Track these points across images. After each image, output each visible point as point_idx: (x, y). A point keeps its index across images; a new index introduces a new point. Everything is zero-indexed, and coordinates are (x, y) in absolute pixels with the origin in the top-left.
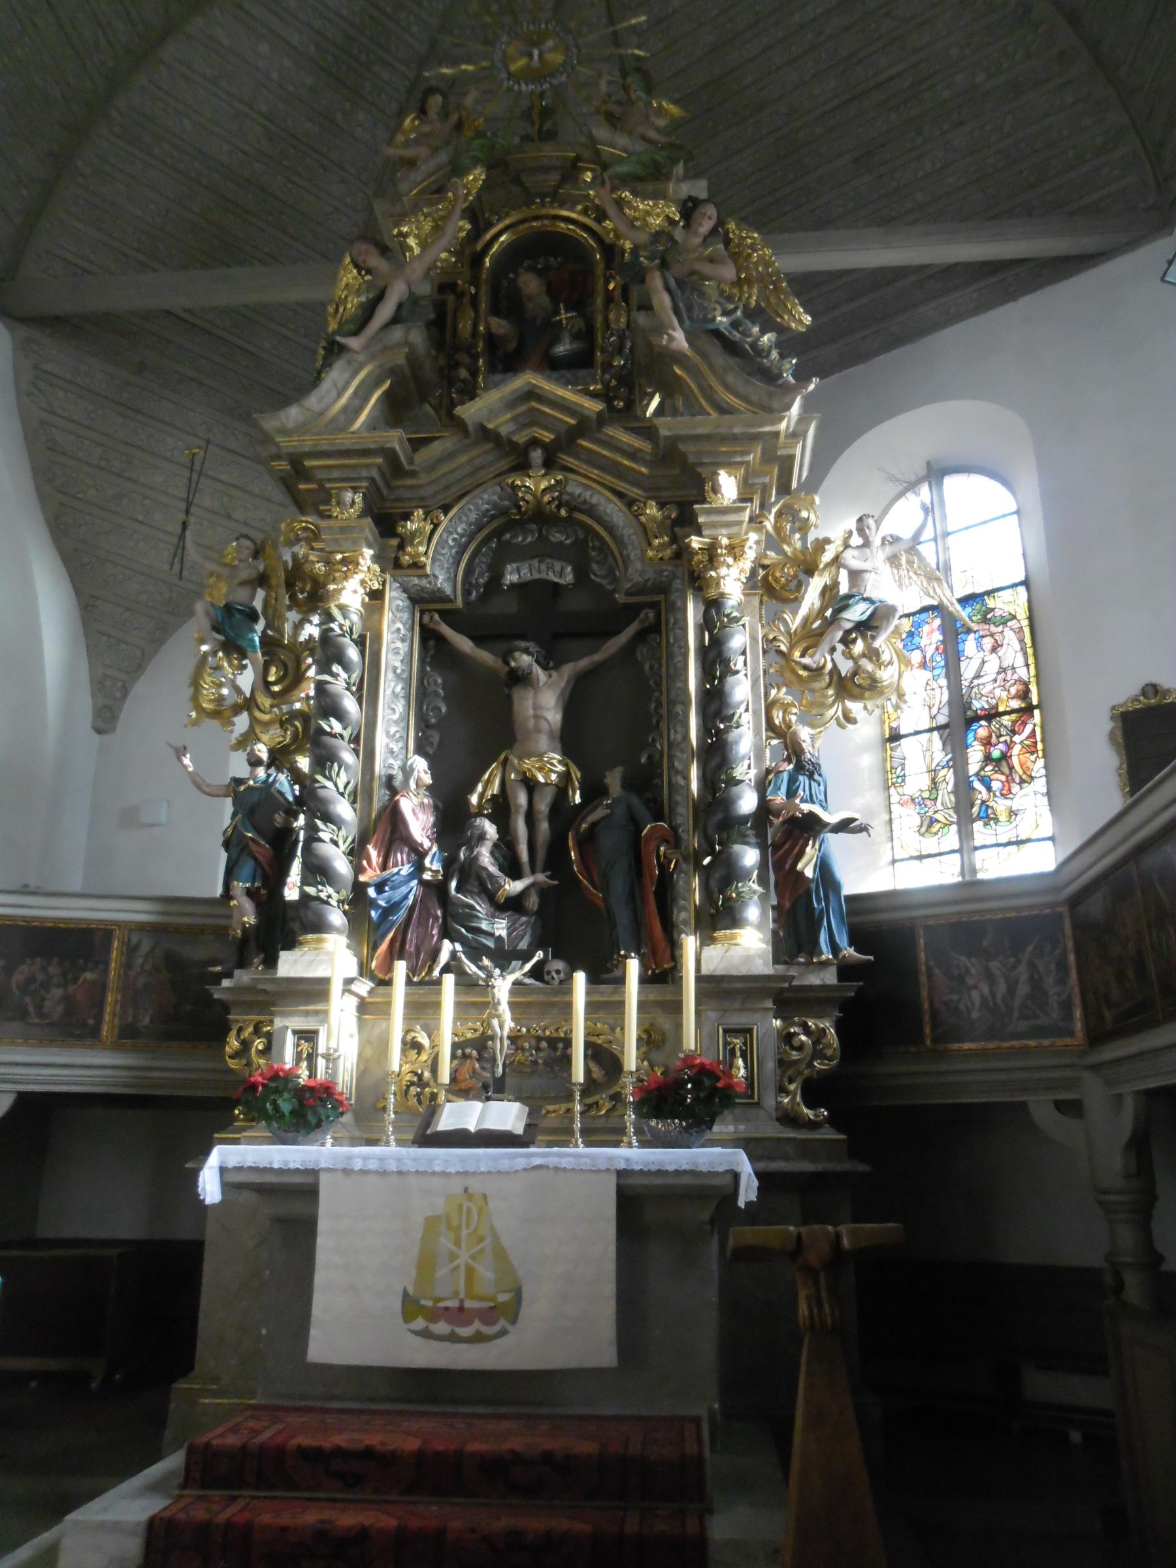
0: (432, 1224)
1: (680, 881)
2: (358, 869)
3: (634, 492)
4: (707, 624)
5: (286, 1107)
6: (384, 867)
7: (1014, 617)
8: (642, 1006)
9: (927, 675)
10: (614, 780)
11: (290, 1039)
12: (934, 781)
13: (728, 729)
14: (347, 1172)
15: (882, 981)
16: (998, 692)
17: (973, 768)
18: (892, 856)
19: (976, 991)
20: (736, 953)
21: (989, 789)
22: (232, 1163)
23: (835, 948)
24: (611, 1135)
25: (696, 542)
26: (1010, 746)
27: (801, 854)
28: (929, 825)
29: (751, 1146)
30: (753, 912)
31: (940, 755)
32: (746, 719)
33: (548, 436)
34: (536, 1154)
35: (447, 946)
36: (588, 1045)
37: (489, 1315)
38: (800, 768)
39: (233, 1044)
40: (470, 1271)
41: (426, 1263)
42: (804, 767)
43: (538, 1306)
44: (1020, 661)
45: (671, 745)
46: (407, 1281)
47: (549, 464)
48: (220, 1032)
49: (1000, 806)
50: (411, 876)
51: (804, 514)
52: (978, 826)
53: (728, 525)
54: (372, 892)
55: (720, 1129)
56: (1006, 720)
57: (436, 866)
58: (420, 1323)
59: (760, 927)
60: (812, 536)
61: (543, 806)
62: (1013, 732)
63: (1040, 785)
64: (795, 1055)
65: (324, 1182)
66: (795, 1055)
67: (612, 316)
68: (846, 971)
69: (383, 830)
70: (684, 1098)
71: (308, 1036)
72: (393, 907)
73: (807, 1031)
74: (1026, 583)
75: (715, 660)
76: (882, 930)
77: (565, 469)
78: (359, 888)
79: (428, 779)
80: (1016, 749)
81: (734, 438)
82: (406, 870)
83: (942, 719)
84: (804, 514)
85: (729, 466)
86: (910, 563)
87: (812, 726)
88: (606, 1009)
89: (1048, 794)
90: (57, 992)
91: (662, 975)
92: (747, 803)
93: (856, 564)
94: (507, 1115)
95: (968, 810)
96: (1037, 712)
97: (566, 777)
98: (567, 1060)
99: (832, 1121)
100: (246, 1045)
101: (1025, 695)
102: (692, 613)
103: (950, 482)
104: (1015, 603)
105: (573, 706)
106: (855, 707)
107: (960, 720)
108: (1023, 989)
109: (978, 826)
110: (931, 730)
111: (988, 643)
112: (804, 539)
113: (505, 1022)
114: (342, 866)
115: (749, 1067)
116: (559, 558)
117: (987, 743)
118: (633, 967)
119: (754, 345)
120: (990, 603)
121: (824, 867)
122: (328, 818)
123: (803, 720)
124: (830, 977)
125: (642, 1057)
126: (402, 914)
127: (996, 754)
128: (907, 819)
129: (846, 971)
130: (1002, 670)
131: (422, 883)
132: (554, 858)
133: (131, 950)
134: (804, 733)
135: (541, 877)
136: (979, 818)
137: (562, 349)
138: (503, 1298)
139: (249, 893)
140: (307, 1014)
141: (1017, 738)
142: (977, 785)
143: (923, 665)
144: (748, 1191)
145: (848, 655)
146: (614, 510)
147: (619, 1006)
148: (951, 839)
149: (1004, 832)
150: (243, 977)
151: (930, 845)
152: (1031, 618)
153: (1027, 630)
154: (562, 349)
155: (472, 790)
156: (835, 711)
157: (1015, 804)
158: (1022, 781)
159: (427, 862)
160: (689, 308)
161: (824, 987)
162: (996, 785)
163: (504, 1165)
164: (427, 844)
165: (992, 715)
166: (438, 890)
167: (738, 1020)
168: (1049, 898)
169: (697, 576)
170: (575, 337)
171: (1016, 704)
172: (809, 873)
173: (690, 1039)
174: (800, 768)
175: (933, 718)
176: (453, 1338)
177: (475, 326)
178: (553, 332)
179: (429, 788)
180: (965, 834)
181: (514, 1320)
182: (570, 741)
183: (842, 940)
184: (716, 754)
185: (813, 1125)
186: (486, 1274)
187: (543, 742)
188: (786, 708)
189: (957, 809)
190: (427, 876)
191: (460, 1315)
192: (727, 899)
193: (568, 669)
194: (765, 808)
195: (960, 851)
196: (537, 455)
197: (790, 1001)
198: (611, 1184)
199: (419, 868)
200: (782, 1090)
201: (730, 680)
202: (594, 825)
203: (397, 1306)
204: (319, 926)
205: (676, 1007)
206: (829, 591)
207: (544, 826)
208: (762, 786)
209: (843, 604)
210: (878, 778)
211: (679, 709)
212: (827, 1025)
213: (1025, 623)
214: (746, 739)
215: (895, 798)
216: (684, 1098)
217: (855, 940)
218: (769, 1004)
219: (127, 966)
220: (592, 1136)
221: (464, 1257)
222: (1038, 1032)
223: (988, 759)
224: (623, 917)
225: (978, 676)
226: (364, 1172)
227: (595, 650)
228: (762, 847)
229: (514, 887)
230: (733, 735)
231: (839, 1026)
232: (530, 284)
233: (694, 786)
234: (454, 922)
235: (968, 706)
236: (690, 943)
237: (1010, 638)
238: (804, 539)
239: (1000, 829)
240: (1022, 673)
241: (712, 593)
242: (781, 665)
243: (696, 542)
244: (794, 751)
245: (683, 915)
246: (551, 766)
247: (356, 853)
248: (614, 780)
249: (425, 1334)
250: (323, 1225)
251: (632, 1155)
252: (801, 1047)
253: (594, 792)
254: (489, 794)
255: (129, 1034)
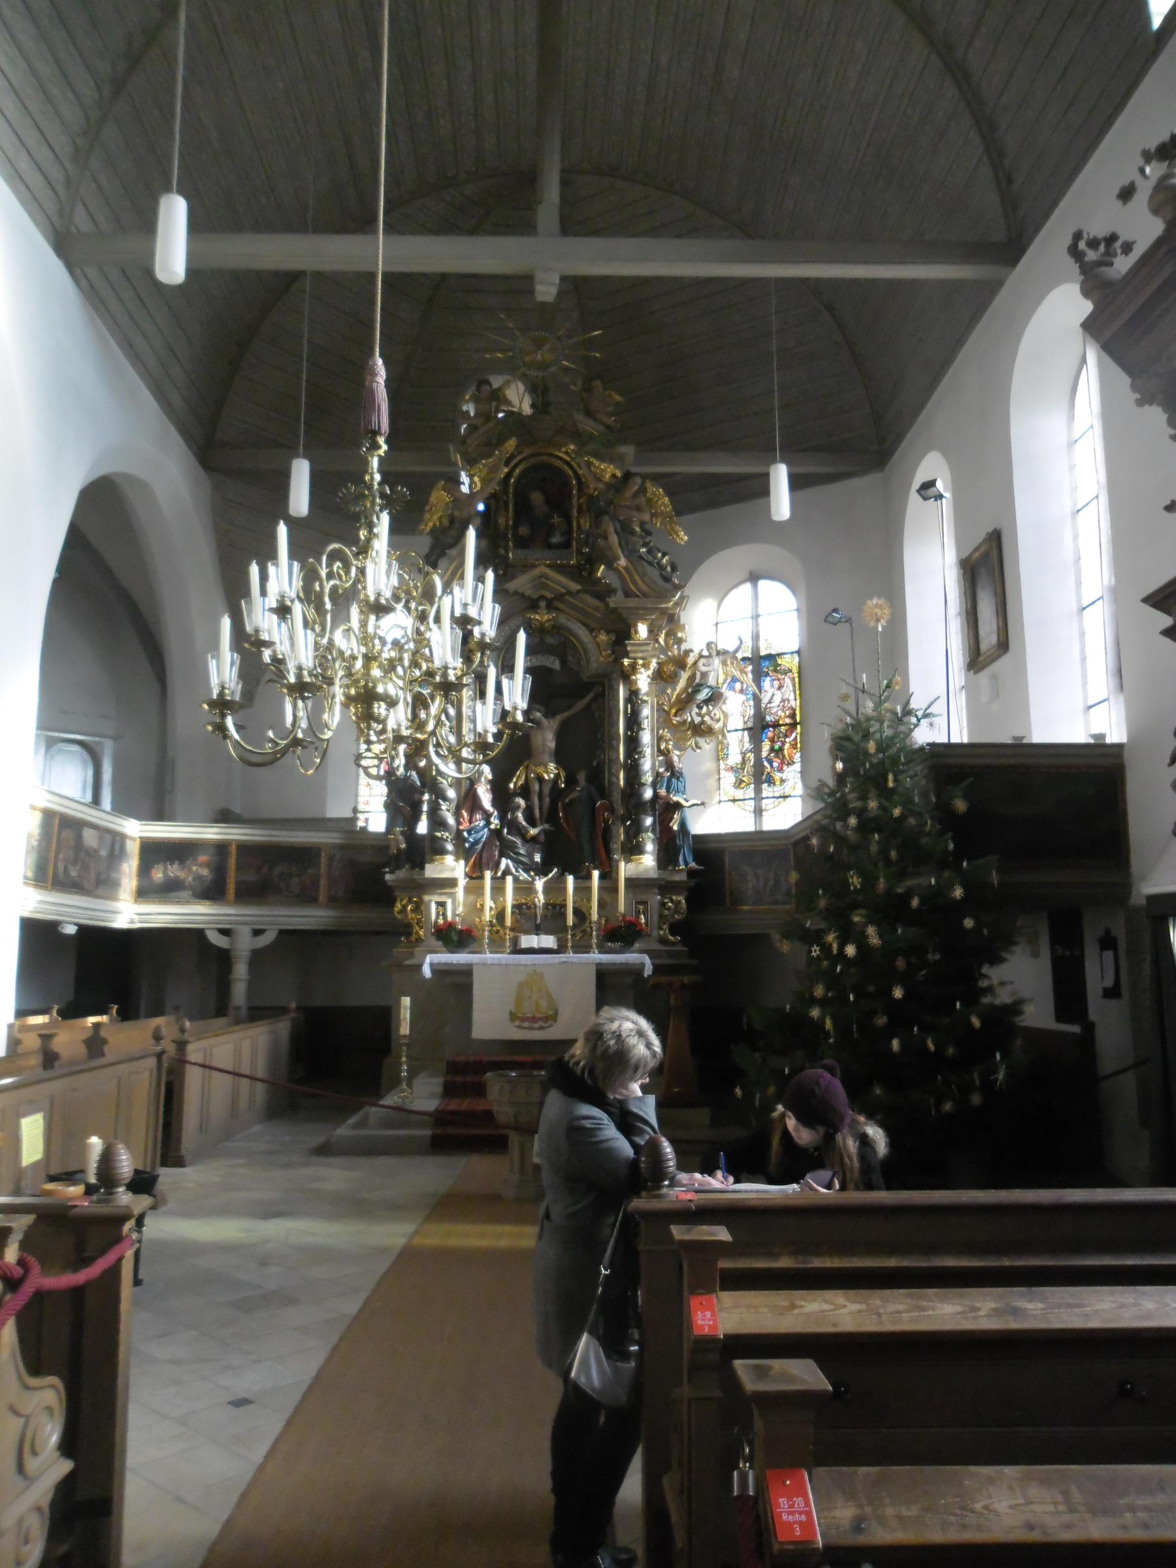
0: (521, 985)
1: (614, 829)
2: (458, 823)
3: (593, 625)
4: (628, 700)
5: (455, 938)
6: (470, 822)
7: (790, 671)
8: (600, 888)
9: (742, 697)
10: (582, 777)
11: (433, 906)
12: (743, 759)
13: (640, 758)
14: (485, 965)
15: (710, 870)
16: (780, 713)
17: (764, 754)
18: (719, 812)
19: (751, 881)
20: (641, 868)
21: (772, 766)
22: (436, 961)
23: (686, 863)
24: (586, 949)
25: (626, 662)
26: (784, 743)
27: (672, 818)
28: (739, 784)
29: (652, 954)
30: (650, 847)
31: (747, 745)
32: (648, 751)
33: (549, 595)
34: (562, 957)
35: (504, 861)
36: (574, 908)
37: (546, 1019)
38: (673, 775)
39: (398, 906)
40: (537, 1003)
41: (520, 999)
42: (675, 774)
43: (564, 1016)
44: (792, 697)
45: (610, 760)
46: (510, 1006)
47: (550, 607)
48: (392, 902)
49: (777, 776)
50: (485, 826)
51: (680, 635)
52: (765, 786)
53: (642, 651)
54: (465, 834)
55: (637, 945)
56: (783, 729)
57: (497, 821)
58: (517, 1023)
59: (652, 854)
60: (684, 647)
61: (546, 790)
62: (786, 736)
63: (797, 767)
64: (666, 912)
65: (475, 968)
66: (666, 912)
67: (582, 521)
68: (691, 873)
69: (468, 803)
70: (621, 934)
71: (441, 905)
72: (476, 842)
73: (672, 901)
74: (798, 652)
75: (634, 722)
76: (712, 853)
77: (557, 609)
78: (459, 833)
79: (490, 777)
80: (787, 746)
81: (646, 609)
82: (482, 823)
83: (750, 725)
84: (680, 635)
85: (643, 619)
86: (732, 663)
87: (680, 750)
88: (583, 890)
89: (801, 772)
90: (296, 880)
91: (609, 876)
92: (648, 794)
93: (704, 669)
94: (549, 941)
95: (760, 777)
96: (799, 727)
97: (557, 776)
98: (563, 916)
99: (683, 942)
100: (405, 907)
101: (793, 716)
102: (622, 692)
103: (762, 583)
104: (790, 662)
105: (560, 736)
106: (701, 741)
107: (759, 726)
108: (771, 882)
109: (765, 786)
110: (743, 730)
111: (776, 683)
112: (679, 649)
113: (541, 898)
114: (451, 821)
115: (646, 919)
116: (552, 654)
117: (772, 741)
118: (596, 874)
119: (659, 563)
120: (779, 661)
121: (683, 824)
122: (445, 799)
123: (676, 747)
124: (683, 877)
125: (600, 916)
126: (479, 846)
127: (777, 747)
128: (728, 778)
129: (691, 873)
130: (783, 701)
131: (490, 830)
132: (551, 817)
133: (331, 858)
134: (675, 756)
135: (546, 826)
136: (765, 782)
137: (555, 540)
138: (551, 1013)
139: (402, 833)
140: (441, 894)
141: (788, 740)
142: (766, 763)
143: (741, 691)
144: (648, 970)
145: (699, 715)
146: (583, 633)
147: (589, 889)
148: (750, 792)
149: (778, 790)
150: (402, 874)
151: (739, 794)
152: (799, 673)
153: (797, 680)
154: (555, 540)
155: (510, 781)
156: (692, 742)
157: (784, 776)
158: (789, 764)
159: (492, 819)
160: (627, 543)
161: (682, 882)
162: (775, 764)
163: (550, 961)
164: (491, 809)
165: (776, 725)
166: (497, 833)
167: (642, 897)
168: (784, 842)
169: (627, 676)
170: (562, 535)
171: (788, 721)
172: (675, 828)
173: (622, 907)
174: (673, 775)
175: (745, 723)
176: (531, 1028)
177: (507, 522)
178: (551, 530)
179: (490, 782)
180: (758, 791)
181: (555, 1021)
182: (560, 757)
183: (690, 859)
184: (633, 770)
185: (673, 944)
186: (544, 1004)
187: (546, 757)
188: (667, 742)
189: (754, 776)
190: (492, 827)
191: (534, 1019)
192: (638, 842)
193: (558, 718)
194: (656, 796)
195: (754, 799)
196: (543, 604)
197: (665, 888)
198: (594, 969)
199: (488, 823)
200: (660, 928)
201: (641, 733)
202: (571, 801)
203: (507, 1016)
204: (442, 852)
205: (615, 890)
206: (692, 678)
207: (547, 800)
208: (654, 785)
209: (697, 690)
210: (713, 754)
211: (614, 742)
212: (682, 899)
213: (796, 675)
214: (647, 764)
215: (722, 766)
216: (621, 934)
217: (695, 860)
218: (656, 891)
219: (330, 866)
220: (578, 949)
221: (534, 998)
222: (776, 902)
223: (772, 750)
224: (586, 846)
225: (770, 702)
226: (492, 964)
227: (570, 707)
228: (654, 816)
229: (533, 832)
230: (642, 760)
231: (687, 899)
232: (537, 498)
233: (622, 783)
234: (506, 849)
235: (764, 719)
236: (622, 864)
237: (788, 682)
238: (679, 649)
239: (776, 789)
240: (793, 703)
241: (633, 688)
242: (663, 718)
243: (626, 662)
244: (670, 766)
245: (616, 846)
246: (551, 771)
247: (457, 814)
248: (582, 777)
249: (520, 1027)
250: (475, 986)
251: (596, 957)
252: (669, 909)
253: (571, 781)
254: (520, 783)
255: (332, 901)
